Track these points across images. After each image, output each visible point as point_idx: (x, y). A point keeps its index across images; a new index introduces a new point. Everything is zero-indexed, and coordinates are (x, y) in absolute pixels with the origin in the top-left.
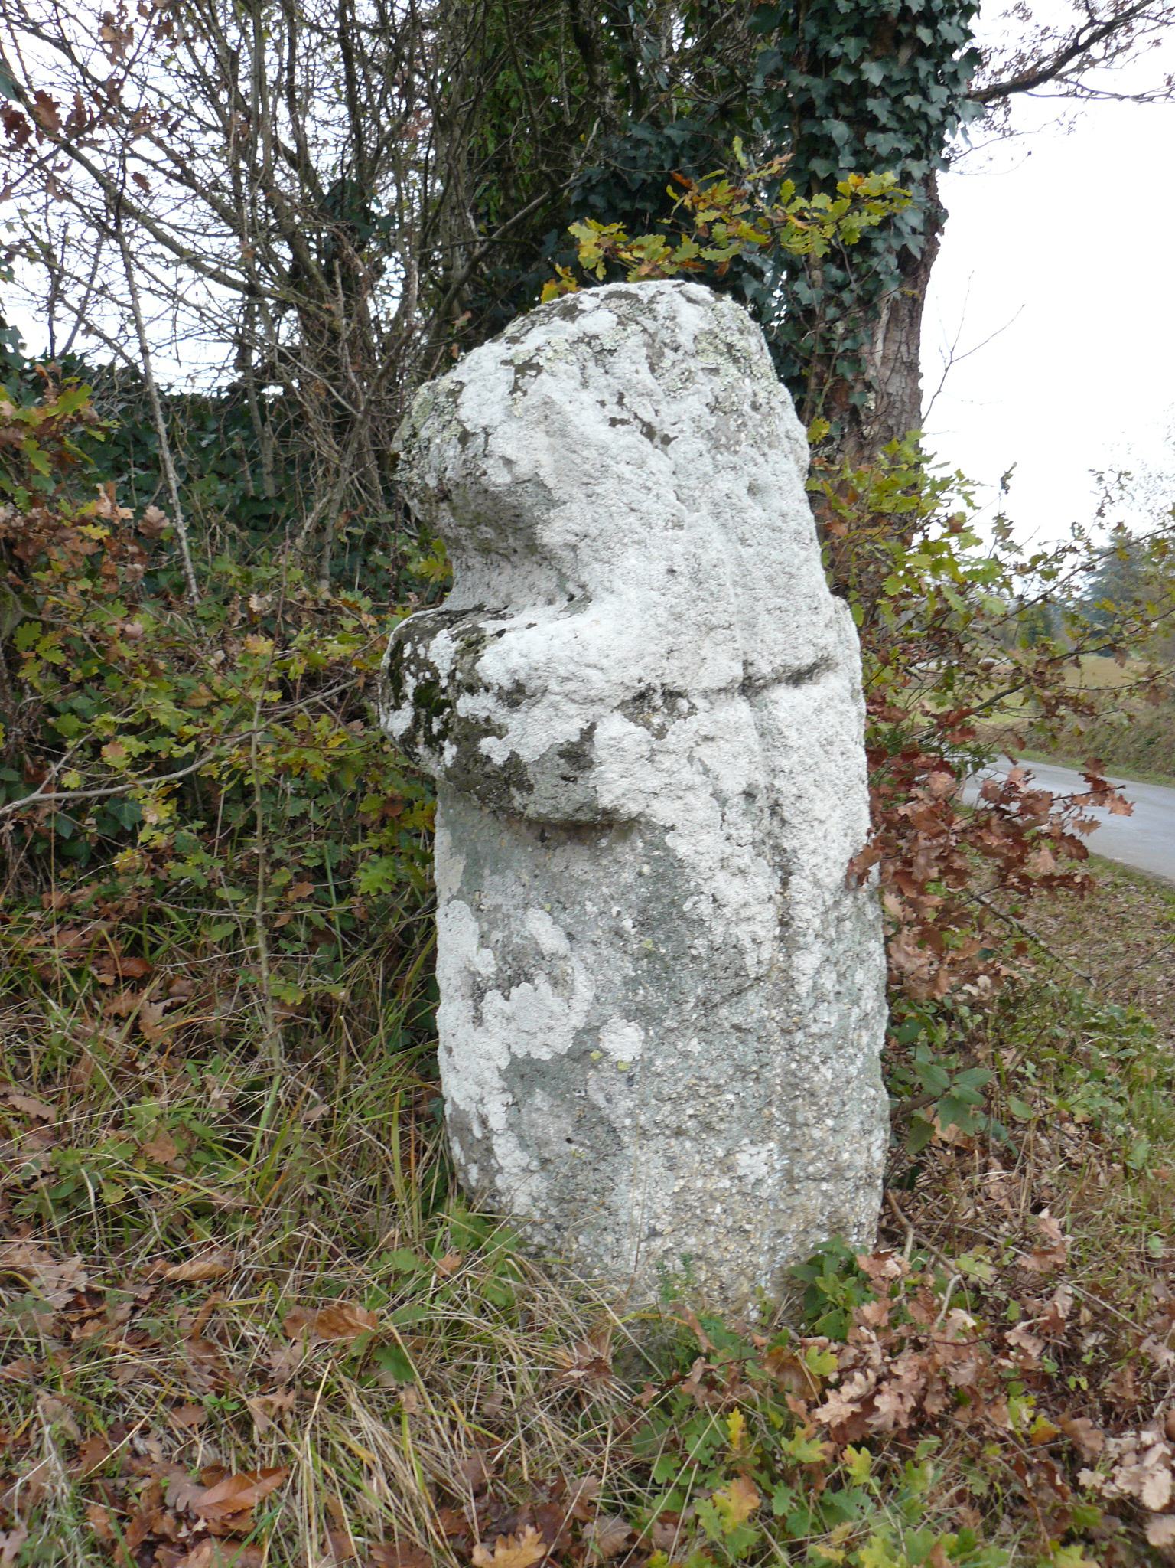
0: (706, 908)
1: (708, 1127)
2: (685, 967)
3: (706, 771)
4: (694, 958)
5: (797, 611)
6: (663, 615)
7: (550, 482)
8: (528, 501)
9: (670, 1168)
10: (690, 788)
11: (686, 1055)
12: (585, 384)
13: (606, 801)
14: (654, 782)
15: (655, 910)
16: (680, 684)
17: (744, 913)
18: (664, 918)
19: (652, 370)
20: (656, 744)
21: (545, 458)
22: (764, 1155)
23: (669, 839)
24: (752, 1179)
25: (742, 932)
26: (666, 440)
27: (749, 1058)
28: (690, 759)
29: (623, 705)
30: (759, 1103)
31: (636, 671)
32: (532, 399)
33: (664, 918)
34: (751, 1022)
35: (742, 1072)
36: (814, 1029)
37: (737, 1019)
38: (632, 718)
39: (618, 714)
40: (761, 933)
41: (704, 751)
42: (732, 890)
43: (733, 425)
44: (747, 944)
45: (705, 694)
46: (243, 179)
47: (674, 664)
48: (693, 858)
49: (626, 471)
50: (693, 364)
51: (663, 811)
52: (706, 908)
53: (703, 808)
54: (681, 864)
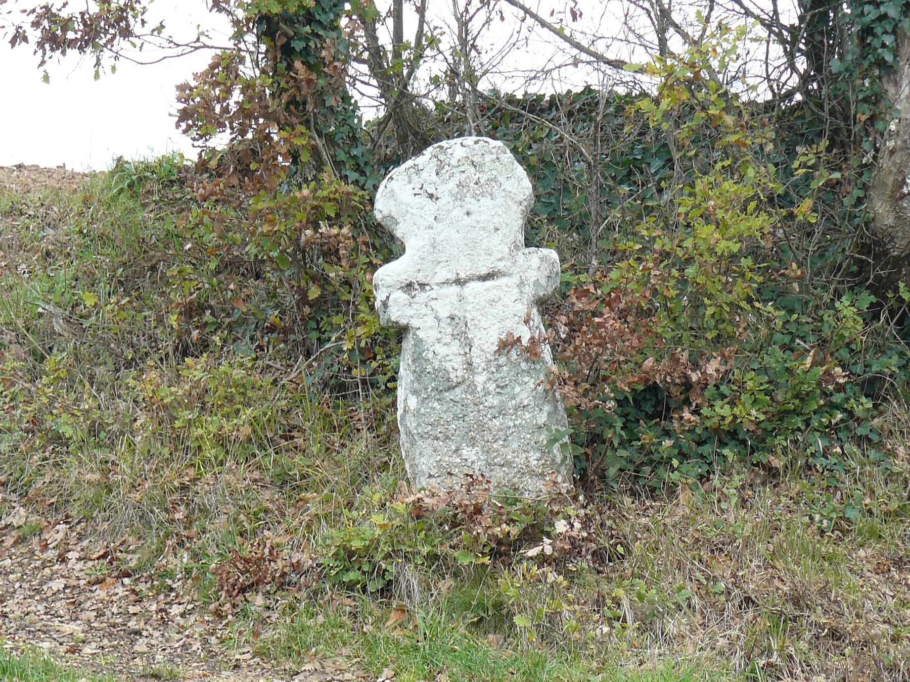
0: (430, 355)
1: (447, 437)
2: (426, 376)
3: (433, 310)
4: (429, 373)
5: (480, 255)
6: (416, 258)
7: (396, 217)
8: (389, 224)
9: (435, 451)
10: (425, 315)
11: (434, 409)
12: (410, 182)
13: (393, 319)
14: (412, 312)
15: (415, 355)
16: (424, 281)
17: (447, 358)
18: (418, 358)
19: (437, 174)
20: (411, 300)
21: (393, 209)
22: (474, 452)
23: (417, 332)
24: (470, 461)
25: (448, 366)
26: (437, 199)
27: (458, 411)
28: (426, 306)
29: (401, 288)
30: (466, 430)
31: (404, 277)
32: (388, 190)
33: (418, 358)
34: (457, 399)
35: (456, 417)
36: (486, 404)
37: (452, 397)
38: (405, 292)
39: (400, 291)
40: (456, 366)
41: (433, 303)
42: (441, 350)
43: (465, 190)
44: (450, 369)
45: (437, 284)
46: (405, 55)
47: (421, 274)
48: (425, 339)
49: (415, 211)
50: (454, 170)
51: (415, 323)
52: (430, 355)
53: (430, 321)
54: (421, 340)
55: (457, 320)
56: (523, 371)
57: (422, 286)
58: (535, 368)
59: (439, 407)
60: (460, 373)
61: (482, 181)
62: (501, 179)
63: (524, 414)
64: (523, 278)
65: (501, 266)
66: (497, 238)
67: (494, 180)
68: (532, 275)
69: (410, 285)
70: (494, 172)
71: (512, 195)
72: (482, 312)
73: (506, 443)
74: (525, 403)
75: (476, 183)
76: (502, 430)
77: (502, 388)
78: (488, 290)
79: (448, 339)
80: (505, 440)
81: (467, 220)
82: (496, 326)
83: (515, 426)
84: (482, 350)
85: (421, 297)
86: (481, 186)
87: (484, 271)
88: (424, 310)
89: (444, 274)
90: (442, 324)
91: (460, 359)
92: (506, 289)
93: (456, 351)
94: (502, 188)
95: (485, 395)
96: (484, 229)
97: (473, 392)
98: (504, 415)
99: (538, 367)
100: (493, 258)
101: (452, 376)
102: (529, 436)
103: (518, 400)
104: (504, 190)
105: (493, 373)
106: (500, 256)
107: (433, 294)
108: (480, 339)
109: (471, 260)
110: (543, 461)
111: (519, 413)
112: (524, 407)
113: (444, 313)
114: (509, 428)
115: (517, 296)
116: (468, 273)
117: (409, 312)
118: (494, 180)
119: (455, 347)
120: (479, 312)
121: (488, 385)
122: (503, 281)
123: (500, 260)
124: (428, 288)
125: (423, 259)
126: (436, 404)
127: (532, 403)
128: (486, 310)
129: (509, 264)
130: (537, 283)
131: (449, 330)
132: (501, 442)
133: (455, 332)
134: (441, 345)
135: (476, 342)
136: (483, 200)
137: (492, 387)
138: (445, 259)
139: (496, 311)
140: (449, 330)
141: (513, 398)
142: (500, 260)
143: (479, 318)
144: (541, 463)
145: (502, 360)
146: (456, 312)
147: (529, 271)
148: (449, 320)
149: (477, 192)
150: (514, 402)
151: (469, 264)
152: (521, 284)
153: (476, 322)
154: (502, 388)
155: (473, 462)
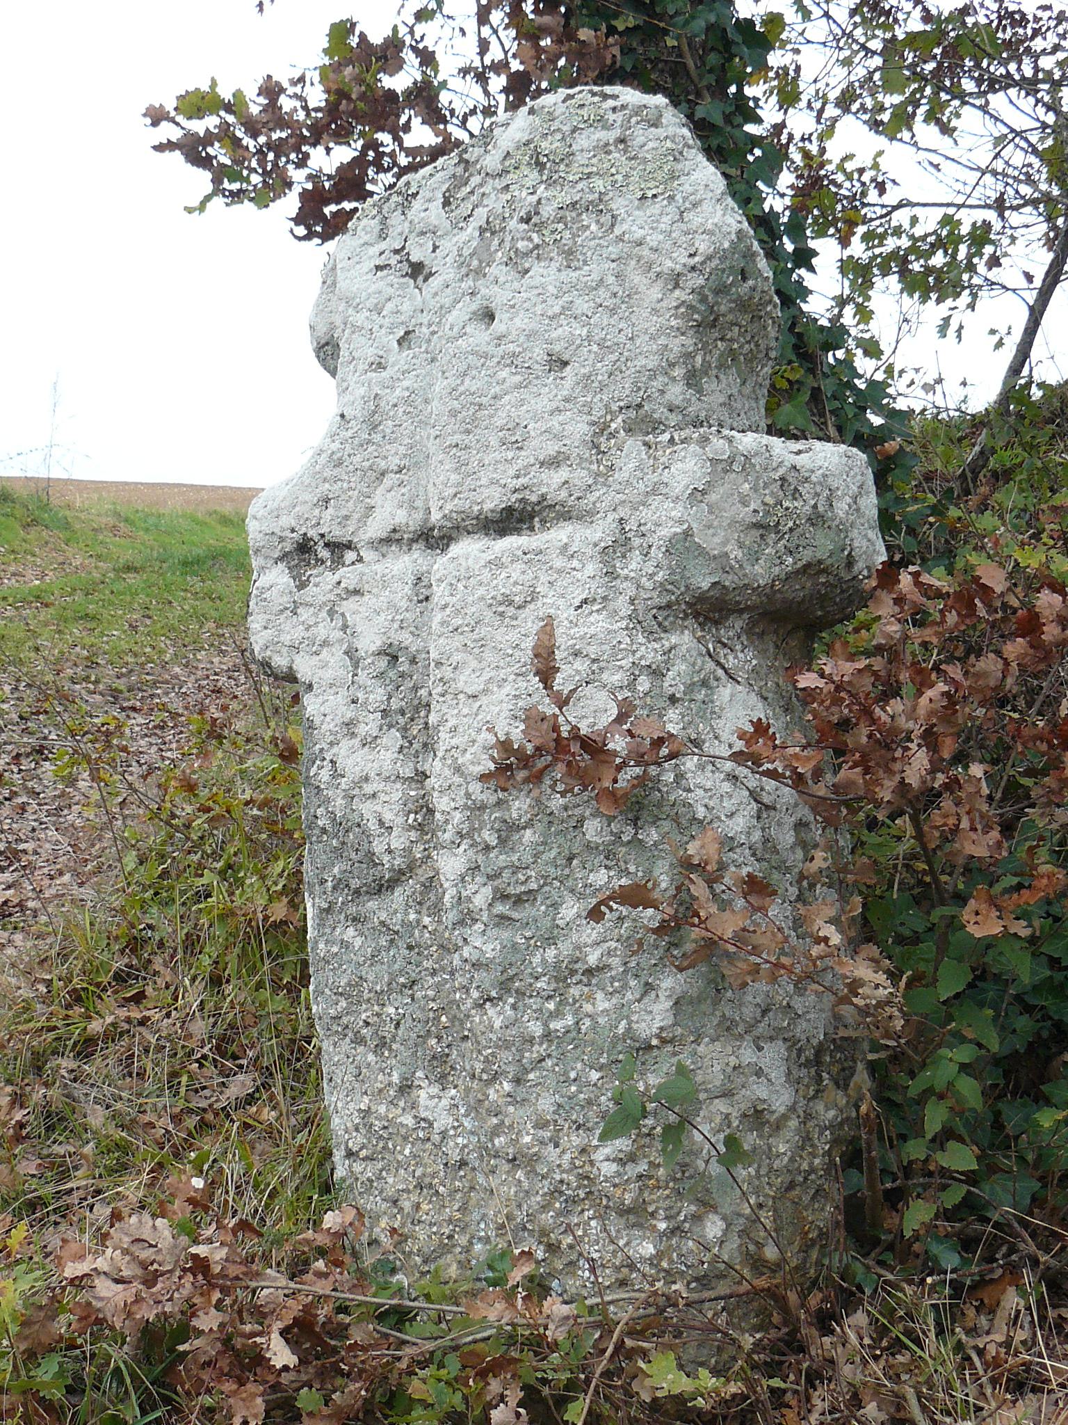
0: (325, 775)
3: (345, 627)
16: (337, 534)
17: (368, 789)
19: (446, 203)
22: (445, 1102)
25: (367, 810)
28: (331, 613)
31: (287, 521)
36: (466, 952)
40: (388, 816)
41: (348, 606)
42: (352, 759)
44: (373, 825)
53: (335, 658)
55: (404, 666)
56: (588, 846)
57: (338, 548)
58: (636, 842)
59: (358, 942)
60: (398, 841)
61: (548, 211)
62: (619, 205)
63: (590, 998)
64: (631, 525)
65: (551, 483)
66: (549, 392)
67: (598, 206)
68: (665, 518)
69: (304, 547)
70: (599, 184)
71: (646, 252)
72: (469, 639)
73: (521, 1093)
74: (593, 959)
75: (527, 220)
76: (506, 1045)
77: (519, 901)
78: (496, 564)
79: (370, 724)
80: (518, 1081)
81: (479, 336)
82: (508, 688)
83: (547, 1036)
84: (458, 770)
85: (324, 582)
86: (539, 227)
87: (493, 501)
88: (325, 629)
89: (389, 511)
90: (362, 676)
91: (396, 793)
92: (559, 563)
93: (387, 767)
94: (618, 231)
95: (461, 923)
96: (511, 361)
97: (436, 910)
98: (520, 994)
99: (651, 835)
100: (526, 457)
101: (378, 847)
102: (595, 1075)
103: (565, 948)
104: (620, 239)
105: (487, 848)
106: (552, 448)
107: (348, 575)
108: (454, 730)
109: (461, 465)
110: (642, 1167)
111: (575, 991)
112: (589, 972)
113: (369, 642)
114: (531, 1041)
115: (596, 588)
116: (449, 507)
117: (292, 632)
118: (598, 206)
119: (387, 756)
120: (458, 641)
121: (472, 888)
122: (560, 534)
123: (554, 462)
124: (350, 556)
125: (339, 463)
126: (351, 932)
127: (615, 961)
128: (483, 631)
129: (580, 477)
130: (683, 545)
131: (378, 695)
132: (507, 1087)
133: (395, 704)
134: (356, 742)
135: (444, 740)
136: (537, 269)
137: (481, 897)
138: (394, 462)
139: (513, 636)
140: (378, 695)
141: (550, 940)
142: (554, 462)
143: (457, 657)
144: (632, 1170)
145: (519, 806)
146: (405, 638)
147: (655, 501)
148: (383, 663)
149: (521, 245)
150: (551, 953)
151: (454, 477)
152: (620, 545)
153: (447, 672)
154: (519, 901)
155: (444, 1134)
